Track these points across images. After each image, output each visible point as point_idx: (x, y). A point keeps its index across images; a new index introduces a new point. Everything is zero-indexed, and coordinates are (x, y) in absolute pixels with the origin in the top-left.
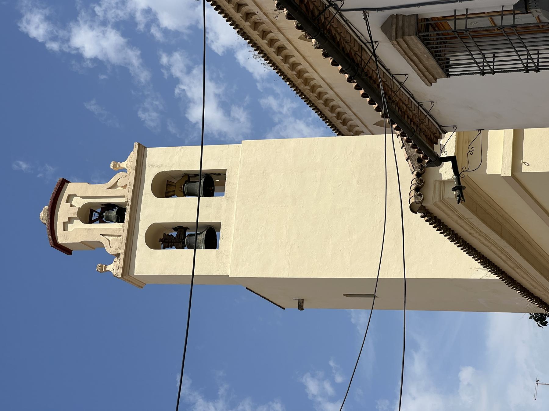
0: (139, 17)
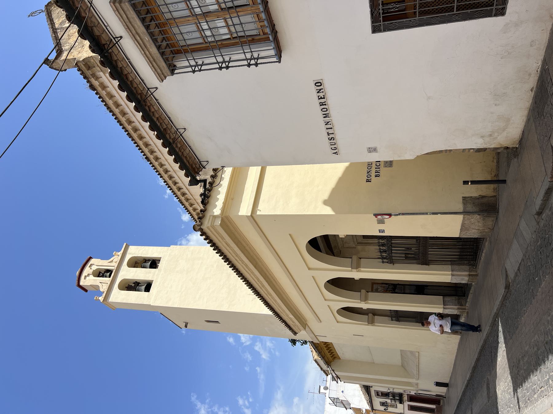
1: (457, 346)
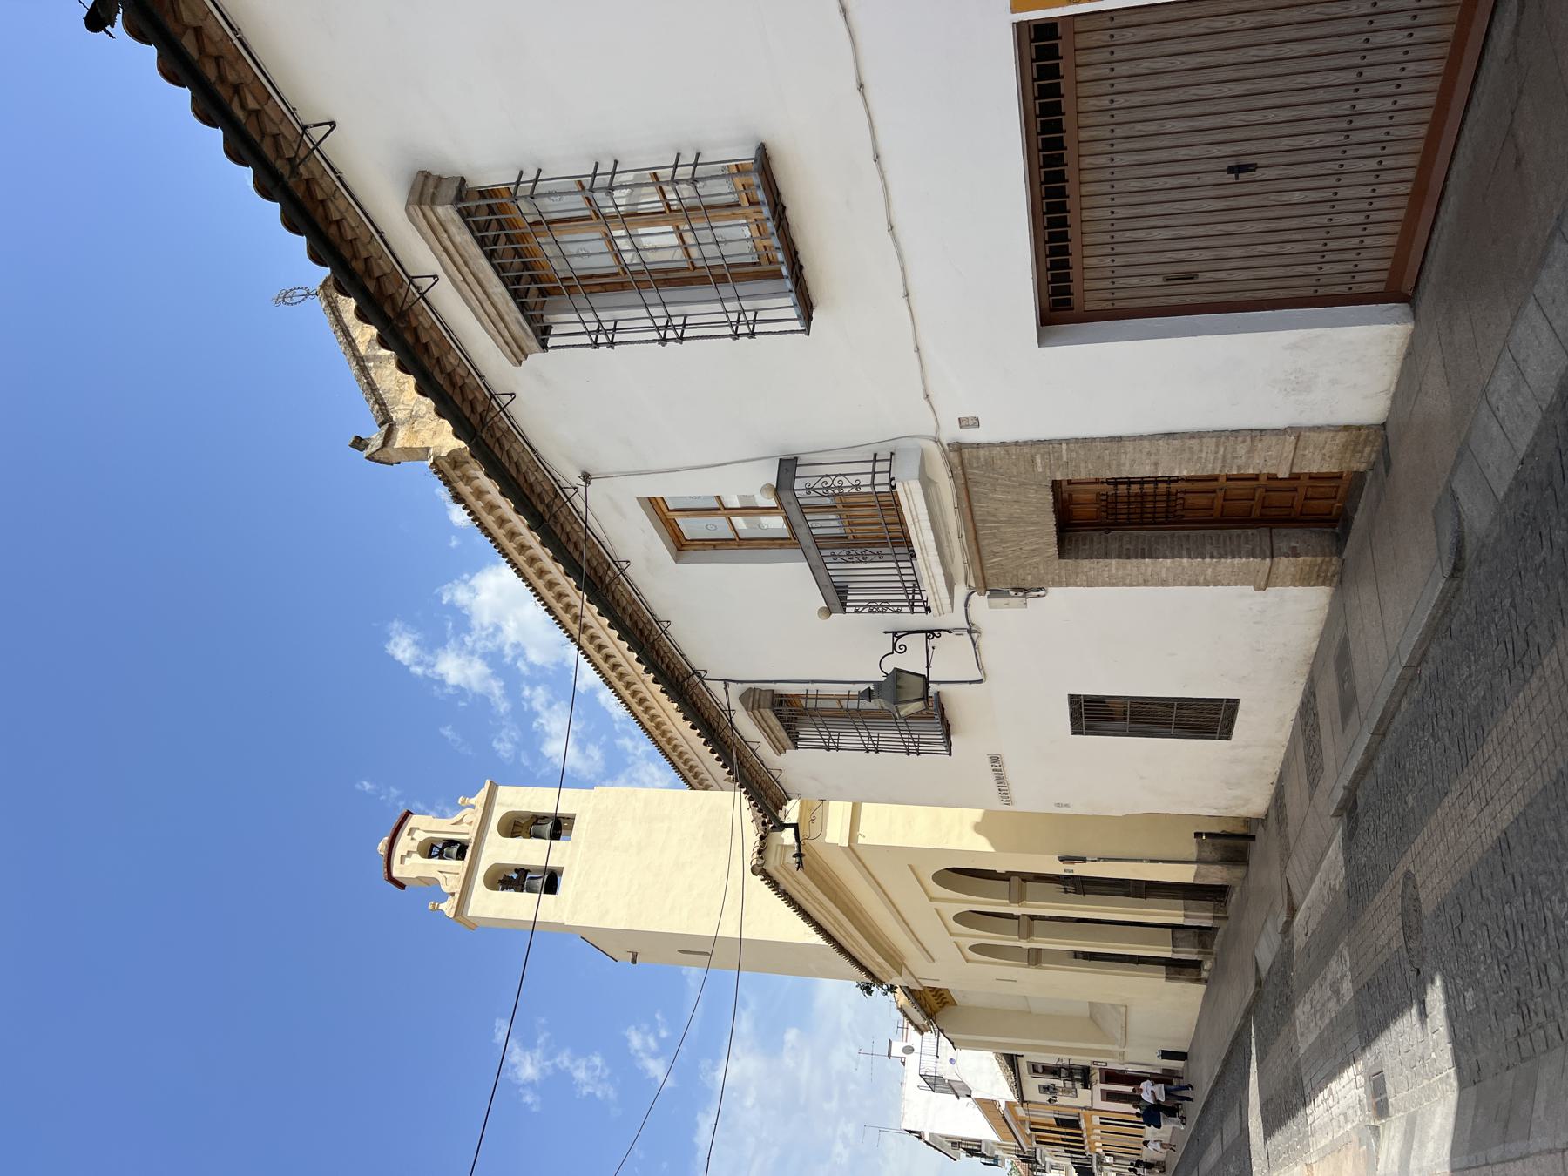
0: (507, 650)
1: (1201, 999)
